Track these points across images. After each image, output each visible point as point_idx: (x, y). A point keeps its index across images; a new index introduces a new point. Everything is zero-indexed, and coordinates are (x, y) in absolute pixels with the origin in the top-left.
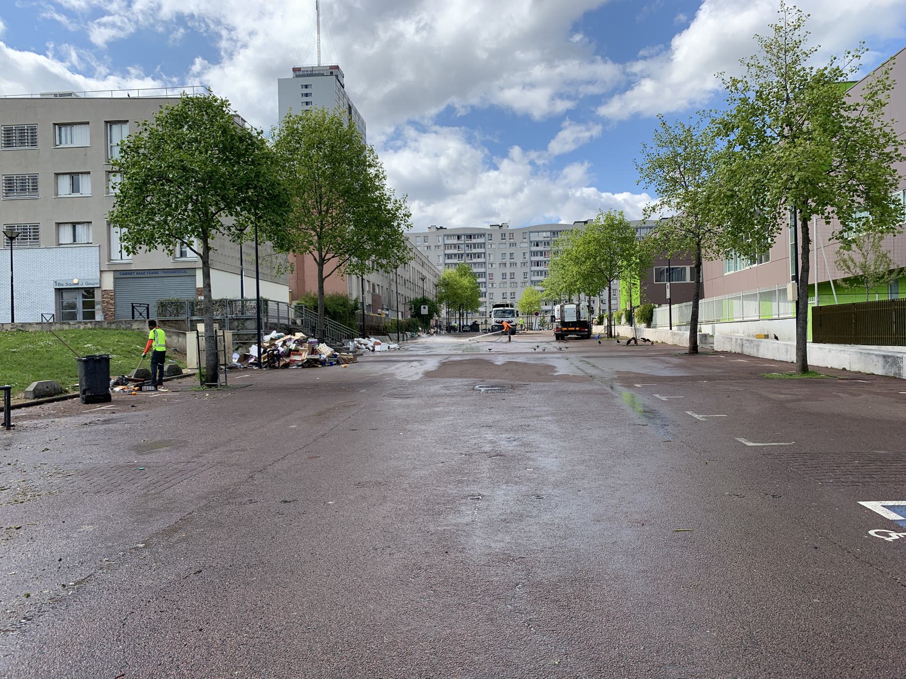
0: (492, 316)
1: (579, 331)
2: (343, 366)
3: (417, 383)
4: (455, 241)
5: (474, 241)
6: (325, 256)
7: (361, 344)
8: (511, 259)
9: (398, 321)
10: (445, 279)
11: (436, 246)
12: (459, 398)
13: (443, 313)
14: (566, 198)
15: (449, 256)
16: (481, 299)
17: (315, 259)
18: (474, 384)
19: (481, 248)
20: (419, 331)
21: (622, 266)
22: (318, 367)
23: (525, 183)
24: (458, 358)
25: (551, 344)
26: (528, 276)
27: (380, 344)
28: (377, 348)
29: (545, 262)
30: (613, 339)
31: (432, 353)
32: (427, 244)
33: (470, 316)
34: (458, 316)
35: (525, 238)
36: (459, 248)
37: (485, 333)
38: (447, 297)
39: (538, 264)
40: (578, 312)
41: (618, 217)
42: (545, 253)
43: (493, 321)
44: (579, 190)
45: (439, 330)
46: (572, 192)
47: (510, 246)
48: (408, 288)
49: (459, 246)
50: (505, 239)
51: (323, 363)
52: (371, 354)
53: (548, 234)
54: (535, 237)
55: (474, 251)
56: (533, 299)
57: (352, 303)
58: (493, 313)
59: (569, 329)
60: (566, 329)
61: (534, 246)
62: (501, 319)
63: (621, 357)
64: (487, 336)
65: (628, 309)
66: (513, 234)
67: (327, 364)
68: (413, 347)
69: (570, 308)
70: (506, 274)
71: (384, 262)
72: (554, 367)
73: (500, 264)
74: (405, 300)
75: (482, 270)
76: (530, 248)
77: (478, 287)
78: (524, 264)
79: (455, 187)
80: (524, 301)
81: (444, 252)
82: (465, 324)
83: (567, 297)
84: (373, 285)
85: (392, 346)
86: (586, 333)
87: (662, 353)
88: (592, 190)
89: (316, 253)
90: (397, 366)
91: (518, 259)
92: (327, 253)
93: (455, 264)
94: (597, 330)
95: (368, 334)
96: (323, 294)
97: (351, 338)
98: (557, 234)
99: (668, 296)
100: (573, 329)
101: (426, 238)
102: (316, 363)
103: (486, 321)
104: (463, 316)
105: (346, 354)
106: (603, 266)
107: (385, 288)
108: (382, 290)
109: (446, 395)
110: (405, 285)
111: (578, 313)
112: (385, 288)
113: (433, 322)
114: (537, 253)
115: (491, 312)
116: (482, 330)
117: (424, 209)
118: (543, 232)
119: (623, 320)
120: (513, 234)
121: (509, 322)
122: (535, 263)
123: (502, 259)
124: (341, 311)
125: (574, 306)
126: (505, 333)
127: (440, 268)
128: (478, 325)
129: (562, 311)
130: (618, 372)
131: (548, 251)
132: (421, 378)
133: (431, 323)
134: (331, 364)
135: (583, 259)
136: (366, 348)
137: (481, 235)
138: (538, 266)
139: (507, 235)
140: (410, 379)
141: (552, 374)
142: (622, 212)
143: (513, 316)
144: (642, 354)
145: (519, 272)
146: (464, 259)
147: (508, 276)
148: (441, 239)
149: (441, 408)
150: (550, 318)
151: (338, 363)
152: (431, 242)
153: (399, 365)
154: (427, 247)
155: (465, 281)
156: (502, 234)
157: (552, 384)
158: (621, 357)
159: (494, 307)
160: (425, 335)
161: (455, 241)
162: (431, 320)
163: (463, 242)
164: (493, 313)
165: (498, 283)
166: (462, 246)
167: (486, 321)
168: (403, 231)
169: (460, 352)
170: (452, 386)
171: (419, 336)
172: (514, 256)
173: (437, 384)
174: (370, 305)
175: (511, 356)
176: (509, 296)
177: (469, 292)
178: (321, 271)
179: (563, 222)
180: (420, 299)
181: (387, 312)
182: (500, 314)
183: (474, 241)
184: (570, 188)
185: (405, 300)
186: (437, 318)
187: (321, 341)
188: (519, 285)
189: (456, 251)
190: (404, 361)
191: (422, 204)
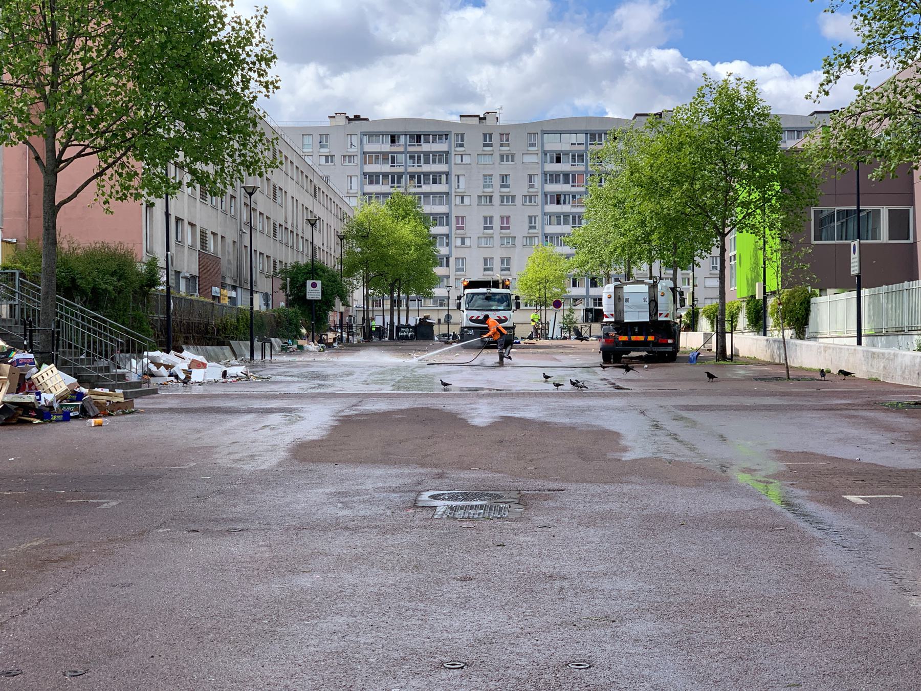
0: (463, 307)
1: (655, 344)
2: (93, 422)
3: (267, 479)
4: (386, 147)
5: (425, 147)
6: (62, 153)
7: (158, 365)
8: (502, 186)
9: (252, 313)
10: (361, 224)
11: (344, 156)
12: (374, 538)
13: (357, 296)
14: (617, 69)
15: (373, 178)
16: (438, 271)
17: (37, 158)
18: (417, 488)
19: (440, 162)
20: (301, 336)
21: (750, 202)
22: (31, 423)
23: (538, 36)
24: (382, 406)
25: (595, 373)
26: (539, 224)
27: (204, 366)
28: (197, 375)
29: (574, 197)
30: (728, 362)
31: (322, 391)
32: (325, 151)
33: (413, 306)
34: (387, 305)
35: (533, 145)
36: (393, 162)
37: (447, 343)
38: (365, 263)
39: (558, 199)
40: (653, 302)
41: (743, 94)
42: (574, 176)
43: (464, 318)
44: (646, 53)
45: (345, 335)
46: (630, 56)
47: (502, 160)
48: (281, 242)
49: (393, 158)
50: (491, 145)
51: (45, 414)
52: (181, 389)
53: (581, 138)
54: (553, 144)
55: (426, 168)
56: (548, 271)
57: (142, 268)
58: (463, 301)
59: (633, 338)
60: (624, 338)
61: (552, 161)
62: (481, 315)
63: (768, 408)
64: (450, 350)
65: (759, 296)
66: (508, 134)
67: (54, 418)
68: (279, 374)
69: (636, 292)
70: (491, 218)
71: (210, 168)
72: (617, 435)
73: (480, 197)
74: (275, 268)
75: (441, 209)
76: (543, 167)
77: (432, 244)
78: (530, 198)
79: (393, 39)
80: (530, 275)
81: (362, 168)
82: (403, 322)
83: (623, 270)
84: (274, 262)
85: (231, 371)
86: (670, 349)
87: (859, 401)
88: (669, 56)
89: (39, 142)
90: (228, 425)
91: (519, 188)
92: (65, 146)
93: (385, 195)
94: (689, 341)
95: (181, 340)
96: (54, 243)
97: (136, 350)
98: (600, 139)
99: (855, 270)
100: (642, 338)
101: (323, 138)
102: (26, 413)
103: (448, 317)
104: (399, 305)
105: (106, 391)
106: (707, 199)
107: (229, 241)
108: (223, 246)
109: (338, 526)
110: (275, 235)
111: (653, 304)
112: (229, 241)
113: (333, 318)
114: (557, 176)
115: (459, 298)
116: (439, 336)
117: (328, 82)
118: (570, 132)
119: (743, 321)
120: (508, 134)
121: (500, 321)
122: (552, 197)
123: (485, 187)
124: (111, 288)
125: (645, 288)
126: (488, 346)
127: (354, 202)
128: (431, 325)
129: (618, 298)
130: (782, 455)
131: (581, 174)
132: (280, 464)
133: (331, 319)
134: (66, 417)
135: (666, 184)
136: (170, 375)
137: (441, 136)
138: (558, 203)
139: (496, 139)
140: (248, 467)
141: (617, 455)
142: (753, 83)
143: (508, 308)
144: (812, 402)
145: (519, 214)
146: (403, 184)
147: (497, 223)
148: (355, 140)
149: (317, 576)
150: (582, 313)
151: (84, 414)
152: (336, 147)
153: (235, 421)
154: (327, 157)
155: (406, 230)
156: (485, 136)
157: (626, 488)
158: (768, 408)
159: (465, 288)
160: (312, 347)
161: (386, 147)
162: (330, 313)
163: (402, 149)
164: (463, 301)
165: (475, 238)
166: (401, 158)
167: (448, 317)
168: (255, 98)
169: (387, 389)
170: (359, 493)
171: (301, 347)
172: (510, 181)
173: (320, 484)
174: (193, 277)
175: (507, 402)
176: (497, 265)
177: (413, 254)
178: (51, 188)
179: (612, 113)
180: (307, 265)
181: (233, 294)
182: (480, 302)
183: (425, 147)
184: (627, 48)
185: (275, 268)
186: (342, 309)
187: (45, 358)
188: (519, 242)
189: (386, 168)
190: (250, 411)
191: (322, 70)
